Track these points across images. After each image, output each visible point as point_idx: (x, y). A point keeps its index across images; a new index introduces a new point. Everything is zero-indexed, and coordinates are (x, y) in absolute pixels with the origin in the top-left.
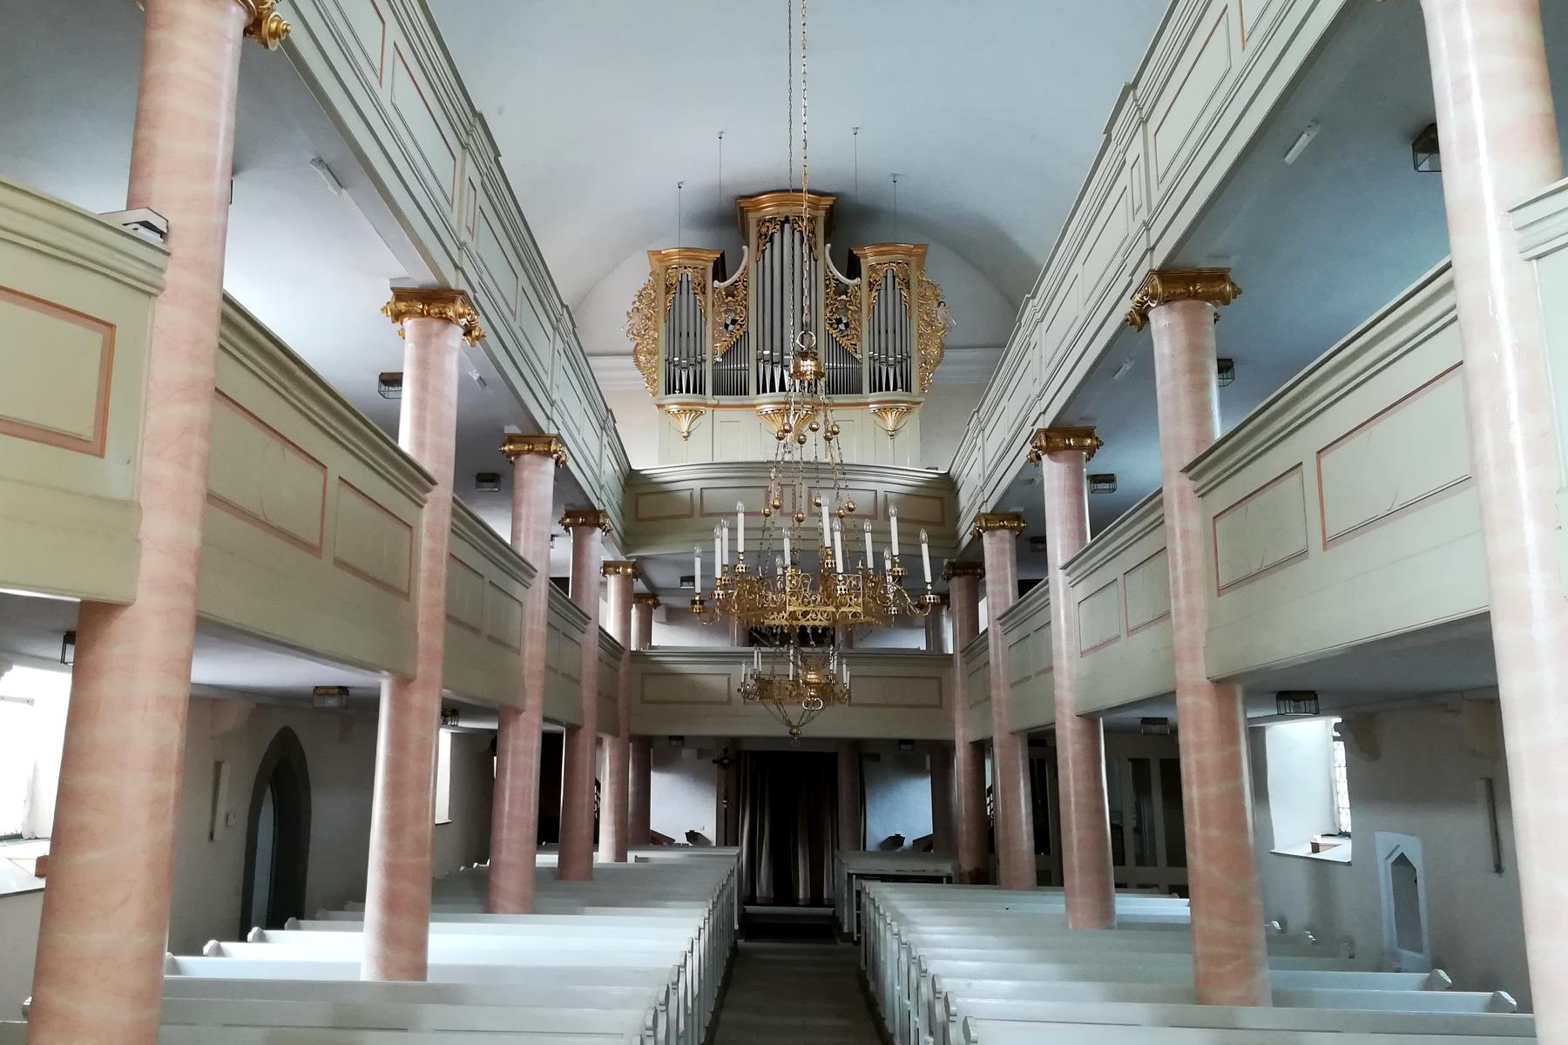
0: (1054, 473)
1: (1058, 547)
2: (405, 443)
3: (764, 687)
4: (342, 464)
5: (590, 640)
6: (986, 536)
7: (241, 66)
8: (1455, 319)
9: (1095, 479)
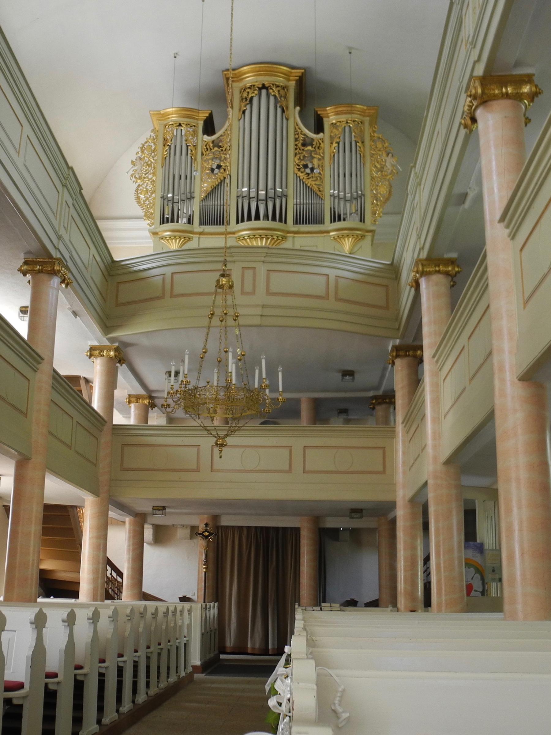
5: (43, 379)
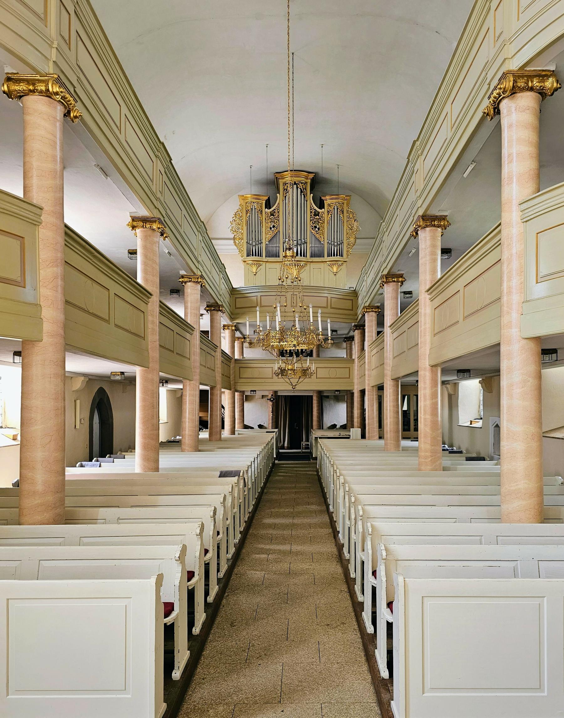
0: (389, 290)
1: (388, 319)
2: (139, 280)
3: (282, 372)
4: (115, 288)
6: (366, 314)
7: (63, 131)
8: (500, 244)
9: (405, 293)
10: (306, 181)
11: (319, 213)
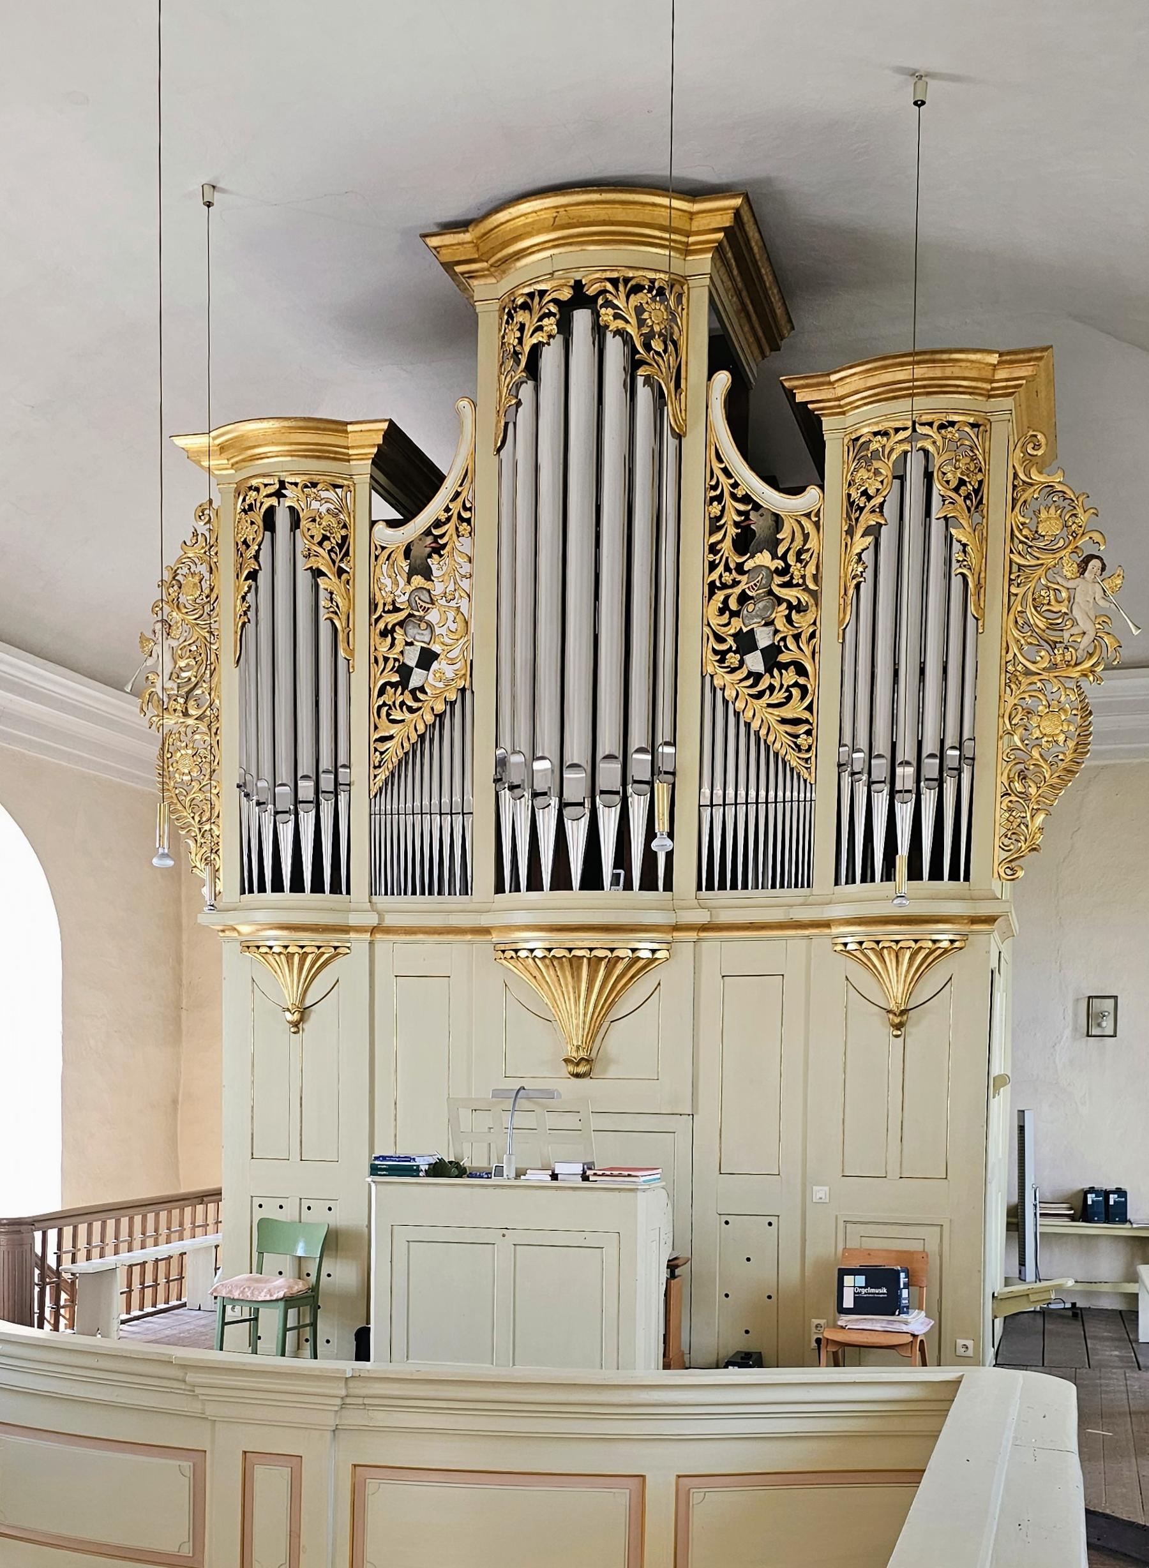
10: (680, 266)
11: (778, 521)
